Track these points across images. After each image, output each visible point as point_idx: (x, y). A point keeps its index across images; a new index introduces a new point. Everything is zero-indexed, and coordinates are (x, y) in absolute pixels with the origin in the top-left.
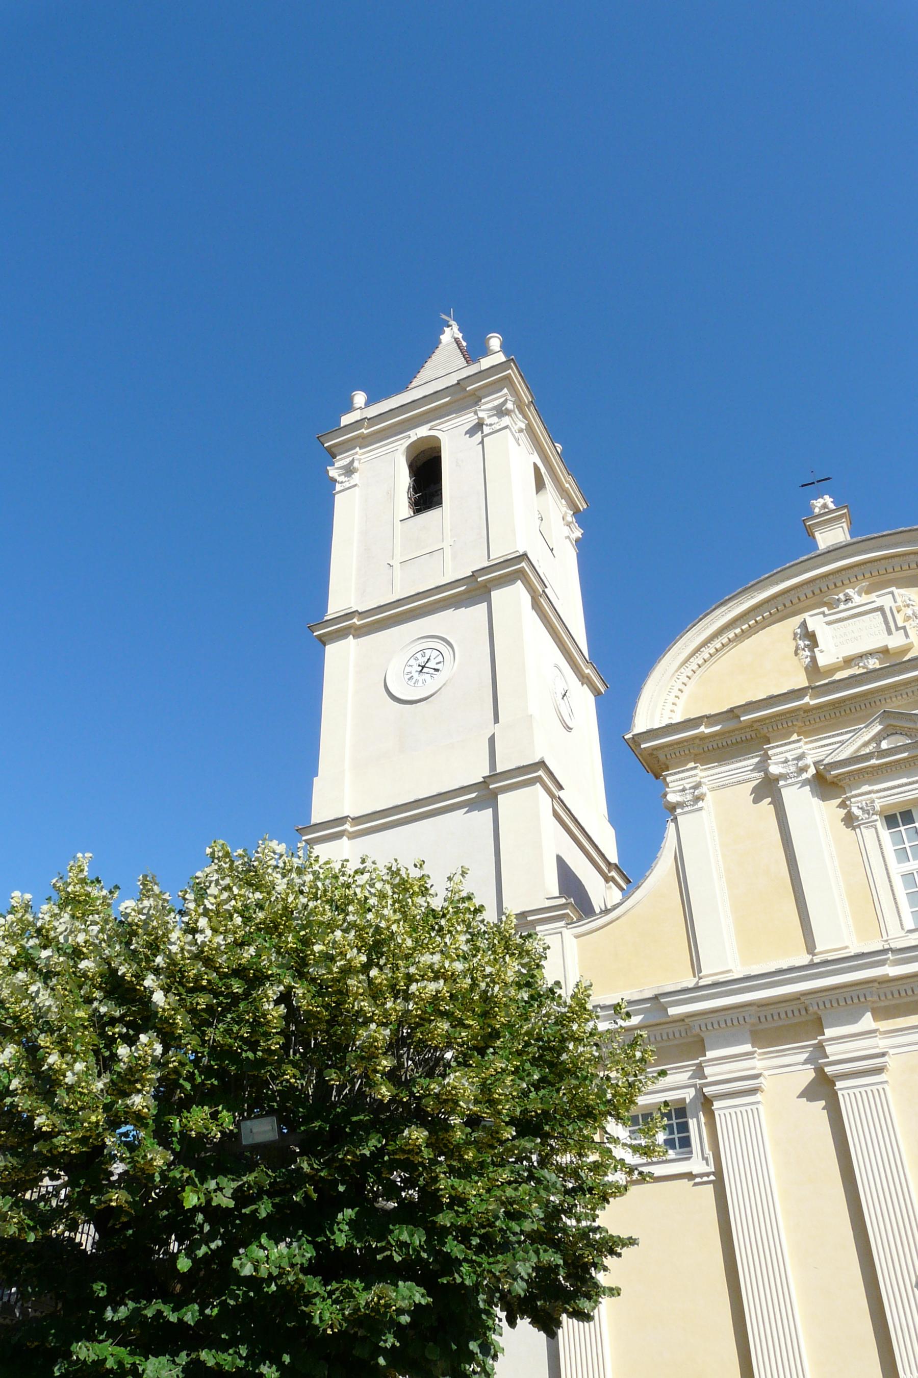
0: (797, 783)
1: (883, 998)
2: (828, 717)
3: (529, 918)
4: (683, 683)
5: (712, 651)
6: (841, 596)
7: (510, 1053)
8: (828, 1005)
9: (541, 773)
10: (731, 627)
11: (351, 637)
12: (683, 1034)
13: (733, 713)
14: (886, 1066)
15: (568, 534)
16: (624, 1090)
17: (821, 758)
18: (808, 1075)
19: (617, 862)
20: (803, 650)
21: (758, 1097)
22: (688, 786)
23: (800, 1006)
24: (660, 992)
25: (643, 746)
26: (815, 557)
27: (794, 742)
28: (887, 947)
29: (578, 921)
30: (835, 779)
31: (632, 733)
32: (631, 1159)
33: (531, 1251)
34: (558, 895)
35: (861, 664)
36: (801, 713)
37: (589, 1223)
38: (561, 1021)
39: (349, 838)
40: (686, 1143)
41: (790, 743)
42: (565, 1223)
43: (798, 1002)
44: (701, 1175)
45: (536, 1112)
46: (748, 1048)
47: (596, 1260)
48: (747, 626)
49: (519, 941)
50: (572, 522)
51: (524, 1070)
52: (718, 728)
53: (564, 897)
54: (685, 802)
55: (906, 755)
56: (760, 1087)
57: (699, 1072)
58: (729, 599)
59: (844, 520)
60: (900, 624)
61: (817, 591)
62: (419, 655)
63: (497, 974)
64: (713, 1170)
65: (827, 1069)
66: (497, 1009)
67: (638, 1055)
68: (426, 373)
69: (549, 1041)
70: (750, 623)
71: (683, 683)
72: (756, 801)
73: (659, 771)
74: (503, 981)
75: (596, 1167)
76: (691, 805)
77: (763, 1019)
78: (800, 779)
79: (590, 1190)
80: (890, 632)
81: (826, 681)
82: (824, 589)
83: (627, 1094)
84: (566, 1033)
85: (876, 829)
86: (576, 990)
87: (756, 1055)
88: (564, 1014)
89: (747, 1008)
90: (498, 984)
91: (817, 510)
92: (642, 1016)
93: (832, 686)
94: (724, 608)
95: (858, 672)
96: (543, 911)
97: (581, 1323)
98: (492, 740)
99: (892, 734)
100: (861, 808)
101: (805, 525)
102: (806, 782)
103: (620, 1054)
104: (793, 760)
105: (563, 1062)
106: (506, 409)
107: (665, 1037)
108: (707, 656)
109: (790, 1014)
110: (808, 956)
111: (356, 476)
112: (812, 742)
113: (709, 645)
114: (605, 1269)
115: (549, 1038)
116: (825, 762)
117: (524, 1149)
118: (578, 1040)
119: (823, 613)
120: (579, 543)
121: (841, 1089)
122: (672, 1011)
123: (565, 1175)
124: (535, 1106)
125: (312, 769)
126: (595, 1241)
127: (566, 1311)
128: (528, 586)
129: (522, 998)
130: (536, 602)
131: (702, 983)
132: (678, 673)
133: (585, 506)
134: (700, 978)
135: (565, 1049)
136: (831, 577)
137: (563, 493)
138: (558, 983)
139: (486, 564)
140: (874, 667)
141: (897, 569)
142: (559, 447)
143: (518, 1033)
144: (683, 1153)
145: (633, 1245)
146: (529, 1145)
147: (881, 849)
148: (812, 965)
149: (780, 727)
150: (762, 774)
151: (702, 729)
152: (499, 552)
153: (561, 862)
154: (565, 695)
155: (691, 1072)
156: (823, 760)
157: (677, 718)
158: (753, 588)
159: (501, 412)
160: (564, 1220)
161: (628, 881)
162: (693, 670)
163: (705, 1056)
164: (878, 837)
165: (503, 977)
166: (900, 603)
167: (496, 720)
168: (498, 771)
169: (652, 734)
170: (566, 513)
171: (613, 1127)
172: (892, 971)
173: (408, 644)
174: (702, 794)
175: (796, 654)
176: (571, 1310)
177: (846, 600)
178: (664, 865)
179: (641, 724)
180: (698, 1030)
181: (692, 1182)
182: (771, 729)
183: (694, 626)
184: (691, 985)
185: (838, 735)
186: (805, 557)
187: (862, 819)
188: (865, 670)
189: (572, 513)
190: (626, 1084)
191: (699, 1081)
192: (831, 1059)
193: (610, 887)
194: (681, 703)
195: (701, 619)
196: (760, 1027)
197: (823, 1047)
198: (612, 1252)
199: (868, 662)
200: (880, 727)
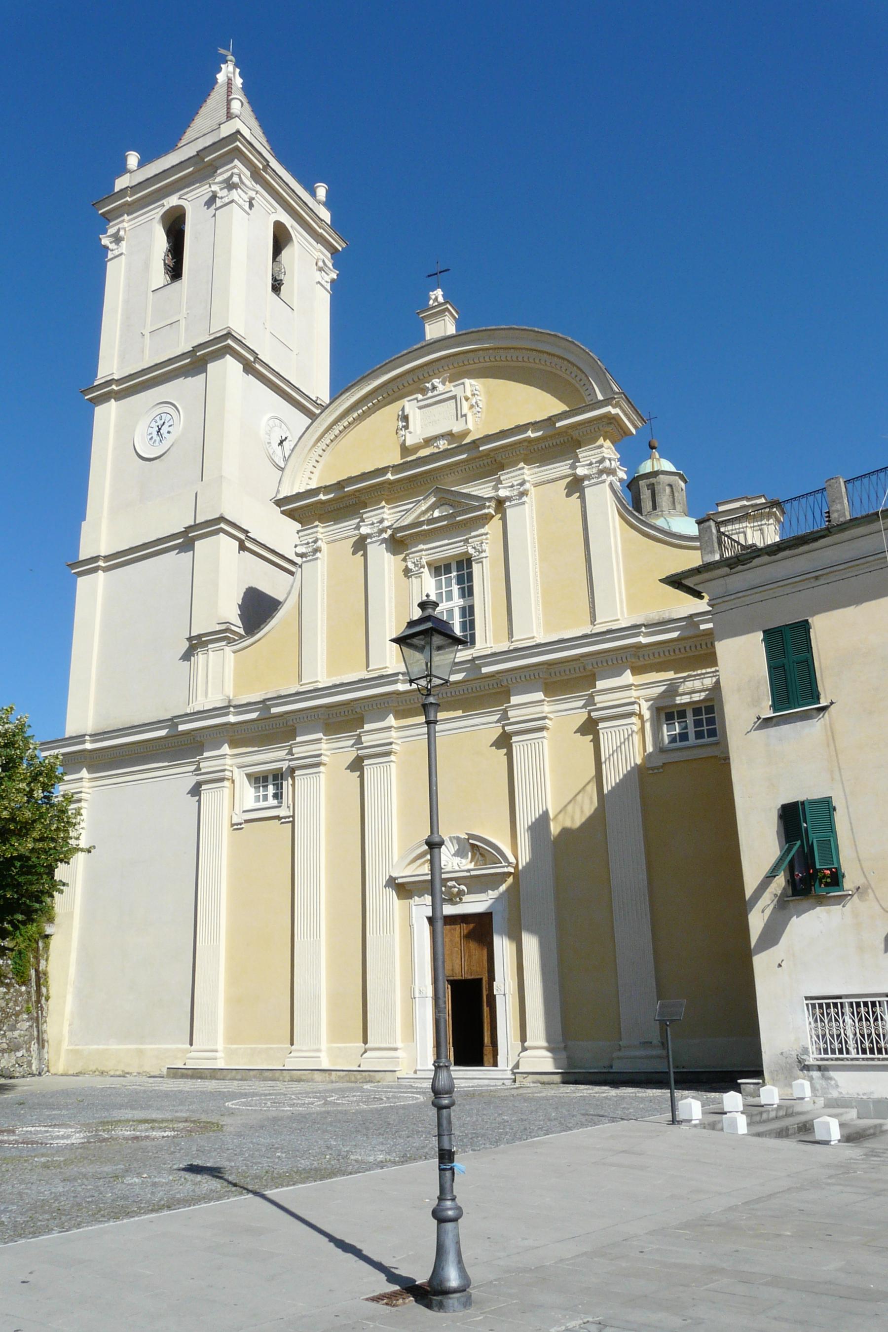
0: (377, 541)
2: (406, 488)
3: (203, 639)
11: (113, 400)
13: (340, 485)
20: (401, 429)
21: (545, 733)
22: (515, 483)
27: (520, 469)
35: (435, 444)
39: (104, 571)
44: (285, 818)
46: (320, 735)
52: (332, 496)
55: (445, 523)
58: (352, 385)
61: (416, 379)
62: (158, 418)
68: (190, 134)
78: (380, 538)
87: (322, 741)
92: (464, 674)
100: (414, 563)
102: (384, 541)
106: (233, 183)
111: (123, 243)
113: (339, 423)
116: (394, 527)
121: (366, 765)
122: (485, 670)
125: (81, 515)
155: (500, 715)
156: (392, 525)
158: (369, 377)
159: (230, 185)
163: (363, 728)
172: (232, 719)
173: (150, 409)
174: (525, 490)
175: (397, 433)
181: (280, 822)
186: (405, 352)
196: (330, 721)
200: (435, 499)
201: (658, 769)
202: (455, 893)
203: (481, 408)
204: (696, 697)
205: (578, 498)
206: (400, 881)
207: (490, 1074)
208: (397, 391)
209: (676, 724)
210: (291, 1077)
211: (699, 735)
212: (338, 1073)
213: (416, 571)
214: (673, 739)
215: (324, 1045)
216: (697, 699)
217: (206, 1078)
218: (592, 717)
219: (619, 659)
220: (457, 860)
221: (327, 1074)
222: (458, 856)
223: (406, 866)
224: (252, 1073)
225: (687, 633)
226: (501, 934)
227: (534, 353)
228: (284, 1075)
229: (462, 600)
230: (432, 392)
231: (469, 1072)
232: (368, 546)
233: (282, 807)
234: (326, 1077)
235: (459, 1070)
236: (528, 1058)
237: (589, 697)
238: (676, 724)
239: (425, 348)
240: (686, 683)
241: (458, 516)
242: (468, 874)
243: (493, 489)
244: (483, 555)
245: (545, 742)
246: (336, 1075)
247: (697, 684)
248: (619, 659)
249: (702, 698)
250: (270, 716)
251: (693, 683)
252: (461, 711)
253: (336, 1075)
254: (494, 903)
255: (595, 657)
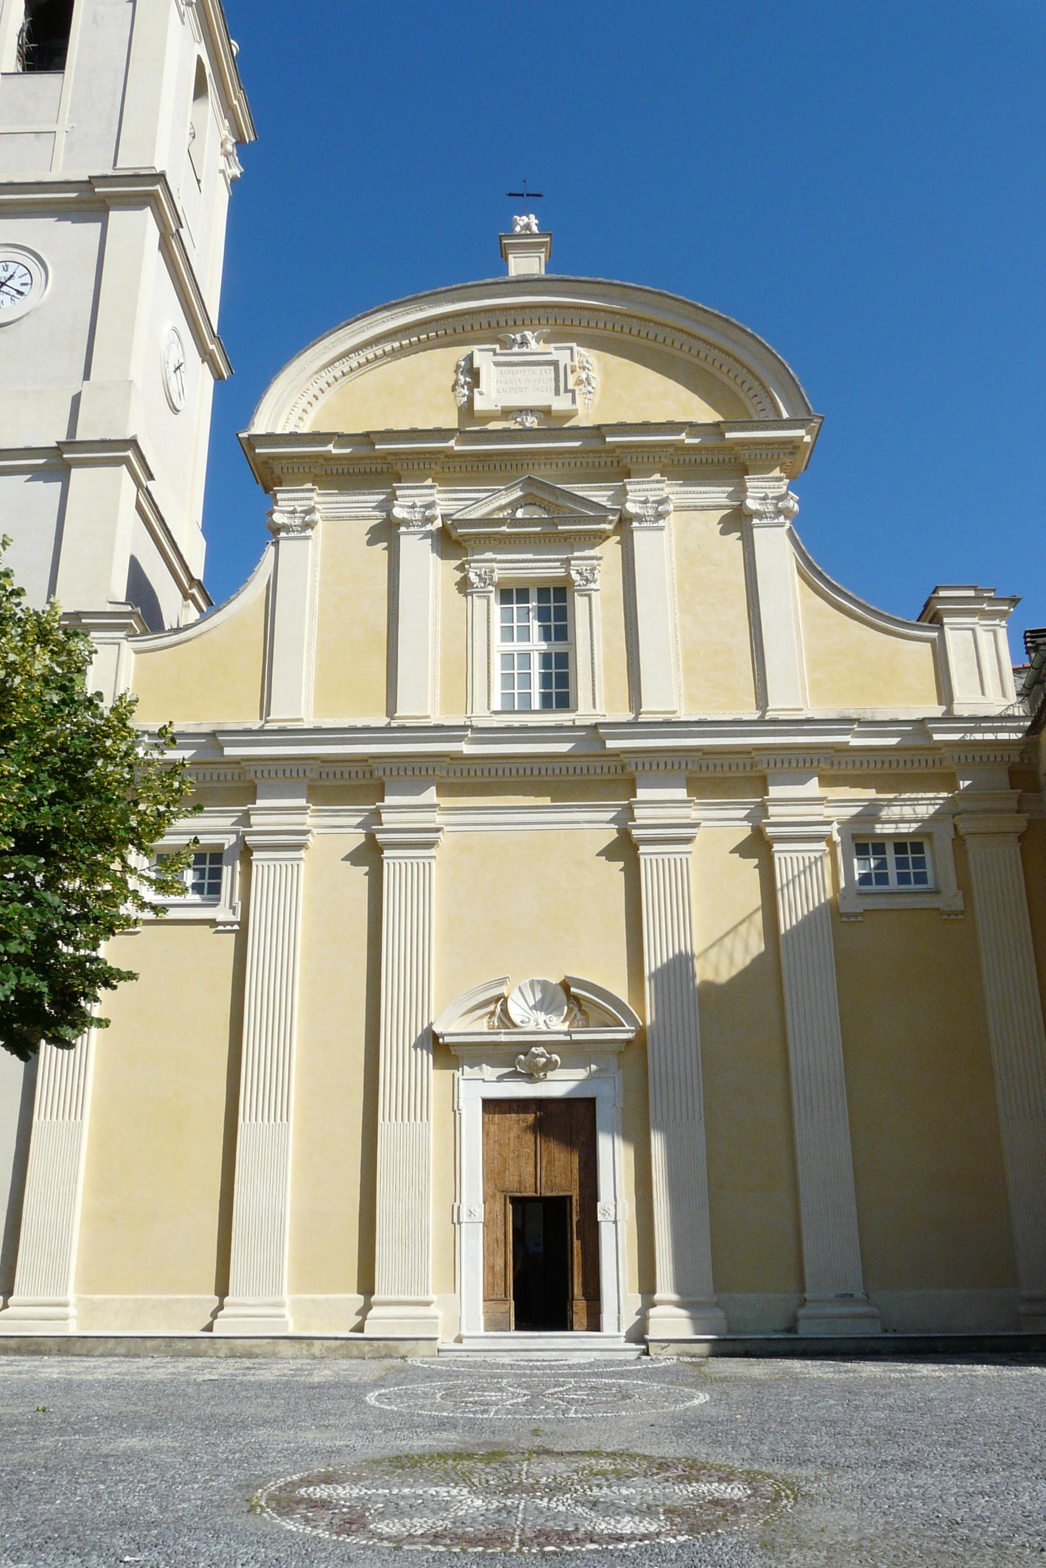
0: (419, 533)
1: (451, 774)
2: (469, 469)
3: (83, 621)
4: (321, 389)
5: (362, 360)
6: (518, 337)
7: (24, 759)
8: (395, 773)
9: (129, 453)
10: (390, 339)
12: (236, 777)
14: (437, 841)
15: (224, 168)
16: (152, 819)
17: (451, 512)
18: (358, 838)
19: (202, 579)
21: (302, 854)
22: (299, 509)
23: (367, 769)
24: (221, 728)
25: (257, 451)
26: (502, 283)
27: (426, 487)
28: (468, 723)
29: (142, 634)
30: (460, 538)
31: (249, 433)
32: (149, 895)
33: (11, 973)
34: (124, 601)
35: (519, 419)
36: (442, 457)
37: (88, 952)
38: (95, 733)
40: (215, 889)
41: (422, 487)
42: (61, 950)
43: (365, 764)
44: (225, 924)
45: (45, 828)
46: (302, 802)
47: (87, 990)
48: (408, 341)
49: (61, 637)
50: (232, 154)
51: (39, 782)
53: (130, 604)
54: (291, 526)
56: (306, 843)
57: (245, 819)
58: (396, 304)
59: (543, 250)
60: (570, 386)
61: (494, 324)
63: (21, 664)
64: (239, 920)
65: (378, 836)
66: (14, 704)
67: (176, 785)
69: (76, 753)
70: (413, 340)
71: (321, 389)
72: (370, 543)
73: (271, 484)
74: (28, 673)
75: (106, 897)
76: (297, 531)
77: (324, 776)
78: (423, 529)
79: (96, 919)
80: (557, 392)
81: (477, 428)
82: (502, 323)
83: (154, 824)
84: (97, 748)
85: (488, 601)
86: (118, 703)
87: (309, 811)
88: (99, 726)
89: (310, 762)
90: (22, 675)
91: (518, 229)
93: (483, 434)
94: (387, 314)
95: (513, 427)
96: (103, 616)
97: (60, 1051)
98: (76, 400)
99: (531, 504)
101: (501, 242)
102: (428, 535)
103: (154, 780)
104: (421, 506)
105: (87, 779)
107: (215, 778)
108: (354, 365)
109: (353, 775)
110: (386, 718)
112: (446, 492)
113: (360, 352)
114: (96, 1000)
115: (75, 750)
116: (454, 517)
117: (26, 868)
118: (109, 758)
119: (494, 351)
120: (235, 184)
121: (387, 858)
122: (228, 751)
123: (69, 901)
124: (45, 817)
126: (91, 971)
127: (45, 1037)
128: (158, 216)
129: (51, 700)
130: (165, 242)
131: (268, 727)
132: (318, 376)
133: (253, 139)
134: (267, 722)
135: (92, 765)
136: (513, 312)
137: (229, 111)
138: (99, 695)
139: (110, 172)
140: (531, 425)
141: (584, 323)
142: (236, 48)
143: (38, 738)
144: (209, 900)
145: (132, 980)
146: (32, 865)
147: (488, 622)
148: (388, 728)
149: (416, 467)
150: (384, 514)
151: (330, 447)
152: (130, 162)
153: (134, 564)
154: (178, 368)
156: (452, 515)
157: (305, 429)
160: (60, 947)
161: (209, 603)
162: (335, 377)
163: (255, 804)
164: (488, 609)
165: (28, 668)
166: (576, 363)
167: (87, 376)
168: (78, 438)
169: (271, 439)
170: (226, 139)
171: (135, 858)
172: (467, 749)
175: (454, 389)
176: (50, 1035)
177: (522, 343)
178: (253, 592)
179: (261, 425)
180: (252, 775)
181: (214, 930)
182: (405, 466)
183: (348, 325)
184: (256, 727)
185: (475, 491)
187: (477, 587)
188: (521, 427)
189: (234, 140)
190: (155, 813)
191: (242, 829)
192: (385, 826)
193: (188, 606)
194: (313, 412)
195: (358, 319)
196: (319, 783)
197: (380, 814)
198: (107, 984)
199: (527, 419)
200: (521, 493)
201: (957, 915)
202: (540, 1065)
203: (593, 388)
204: (904, 828)
205: (618, 543)
206: (448, 1039)
207: (592, 1343)
208: (451, 335)
209: (872, 860)
210: (231, 1349)
211: (903, 879)
212: (327, 1343)
213: (481, 588)
214: (865, 879)
215: (287, 1297)
216: (906, 831)
217: (49, 1353)
218: (376, 840)
219: (808, 761)
220: (541, 1016)
221: (304, 1345)
222: (541, 1011)
223: (462, 1015)
224: (149, 1343)
225: (910, 742)
226: (612, 1132)
227: (685, 336)
228: (218, 1346)
229: (543, 643)
230: (519, 348)
231: (554, 1340)
232: (401, 537)
233: (218, 907)
234: (302, 1348)
235: (539, 1337)
236: (663, 1317)
237: (244, 814)
238: (872, 860)
239: (522, 284)
240: (893, 808)
241: (562, 525)
242: (568, 1038)
243: (727, 497)
244: (592, 586)
245: (302, 864)
246: (322, 1345)
247: (907, 811)
248: (808, 761)
249: (911, 830)
250: (223, 760)
251: (901, 810)
252: (549, 798)
253: (322, 1345)
254: (578, 1086)
255: (509, 761)
